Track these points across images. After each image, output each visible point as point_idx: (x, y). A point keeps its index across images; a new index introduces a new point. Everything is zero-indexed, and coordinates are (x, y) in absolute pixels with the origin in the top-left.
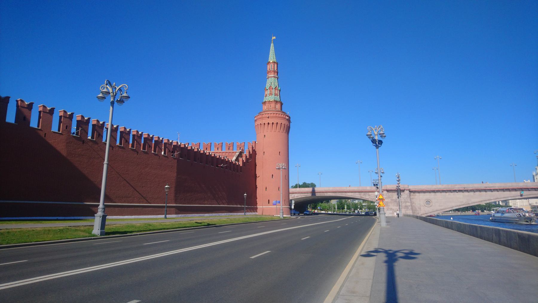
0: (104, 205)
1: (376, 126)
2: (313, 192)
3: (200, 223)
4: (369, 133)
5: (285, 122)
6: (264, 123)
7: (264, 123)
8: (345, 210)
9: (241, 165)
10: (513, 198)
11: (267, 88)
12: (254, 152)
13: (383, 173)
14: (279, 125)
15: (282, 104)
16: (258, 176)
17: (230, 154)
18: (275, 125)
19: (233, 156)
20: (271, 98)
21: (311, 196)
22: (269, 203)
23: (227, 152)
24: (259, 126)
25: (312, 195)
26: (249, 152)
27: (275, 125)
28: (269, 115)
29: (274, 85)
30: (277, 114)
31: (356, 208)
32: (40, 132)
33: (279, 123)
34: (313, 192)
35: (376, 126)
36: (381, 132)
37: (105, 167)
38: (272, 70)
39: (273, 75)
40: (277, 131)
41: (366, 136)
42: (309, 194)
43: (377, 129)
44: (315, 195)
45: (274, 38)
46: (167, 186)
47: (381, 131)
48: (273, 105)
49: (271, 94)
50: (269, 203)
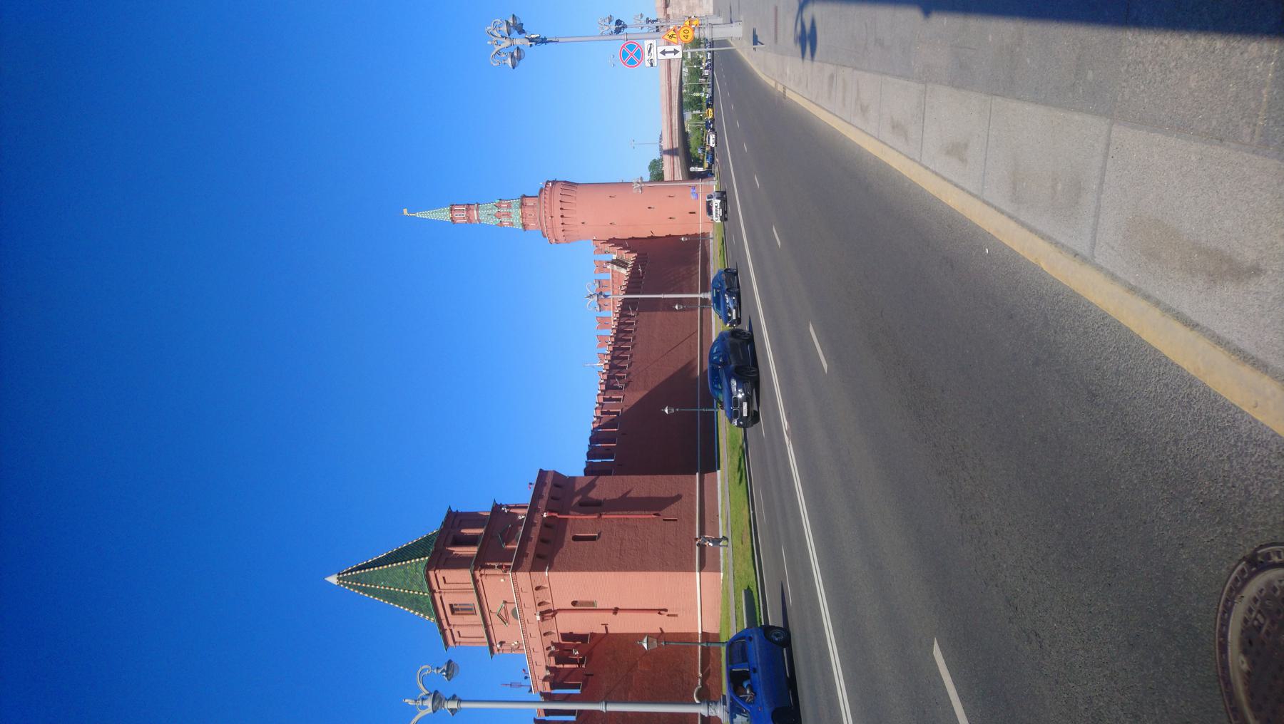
0: (701, 293)
1: (489, 43)
2: (672, 152)
3: (720, 252)
4: (509, 61)
5: (558, 189)
6: (562, 224)
7: (562, 224)
8: (703, 95)
9: (636, 254)
10: (762, 522)
11: (498, 221)
12: (609, 241)
13: (642, 16)
14: (565, 199)
15: (524, 196)
16: (650, 235)
17: (616, 280)
18: (564, 206)
19: (619, 273)
20: (516, 213)
21: (678, 158)
22: (694, 213)
23: (613, 286)
24: (567, 233)
25: (677, 154)
26: (612, 246)
27: (564, 206)
28: (548, 216)
29: (492, 209)
30: (545, 202)
31: (698, 73)
32: (624, 410)
33: (560, 198)
34: (672, 152)
35: (489, 43)
36: (504, 28)
37: (613, 708)
38: (465, 214)
39: (475, 212)
40: (574, 208)
41: (516, 68)
42: (675, 160)
43: (495, 39)
44: (676, 149)
45: (405, 212)
46: (645, 645)
47: (501, 29)
48: (528, 211)
49: (508, 215)
50: (694, 213)
